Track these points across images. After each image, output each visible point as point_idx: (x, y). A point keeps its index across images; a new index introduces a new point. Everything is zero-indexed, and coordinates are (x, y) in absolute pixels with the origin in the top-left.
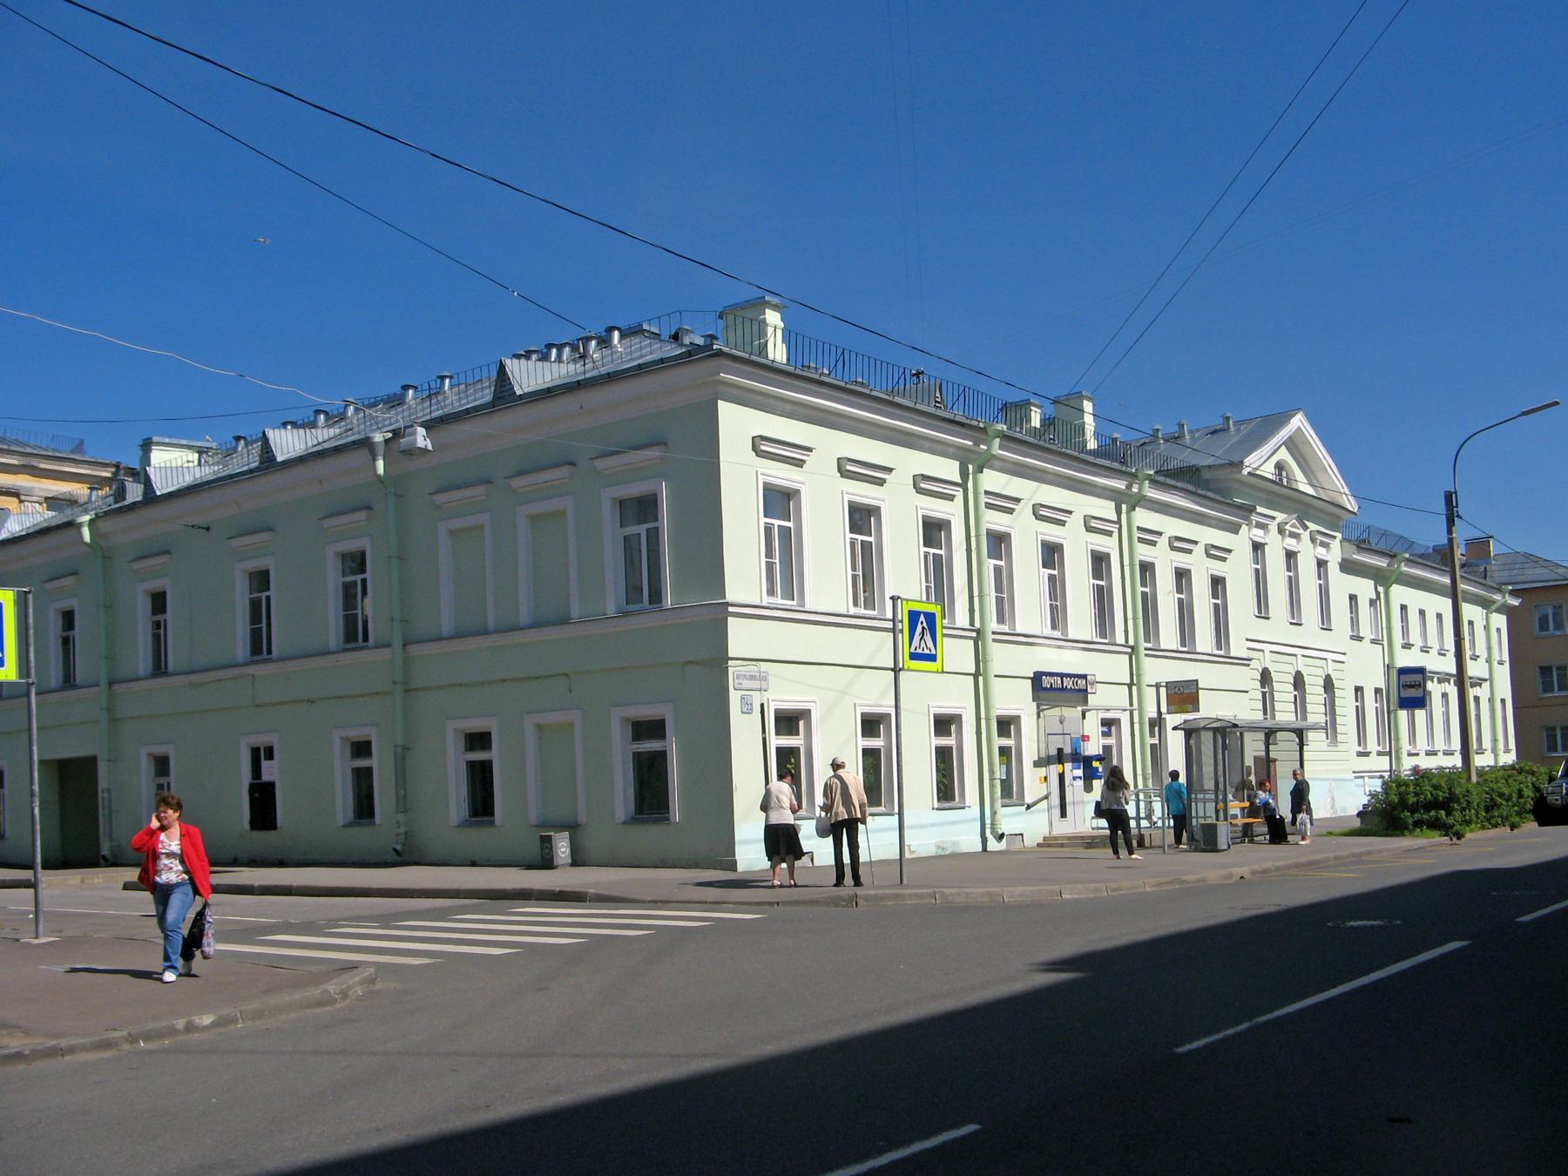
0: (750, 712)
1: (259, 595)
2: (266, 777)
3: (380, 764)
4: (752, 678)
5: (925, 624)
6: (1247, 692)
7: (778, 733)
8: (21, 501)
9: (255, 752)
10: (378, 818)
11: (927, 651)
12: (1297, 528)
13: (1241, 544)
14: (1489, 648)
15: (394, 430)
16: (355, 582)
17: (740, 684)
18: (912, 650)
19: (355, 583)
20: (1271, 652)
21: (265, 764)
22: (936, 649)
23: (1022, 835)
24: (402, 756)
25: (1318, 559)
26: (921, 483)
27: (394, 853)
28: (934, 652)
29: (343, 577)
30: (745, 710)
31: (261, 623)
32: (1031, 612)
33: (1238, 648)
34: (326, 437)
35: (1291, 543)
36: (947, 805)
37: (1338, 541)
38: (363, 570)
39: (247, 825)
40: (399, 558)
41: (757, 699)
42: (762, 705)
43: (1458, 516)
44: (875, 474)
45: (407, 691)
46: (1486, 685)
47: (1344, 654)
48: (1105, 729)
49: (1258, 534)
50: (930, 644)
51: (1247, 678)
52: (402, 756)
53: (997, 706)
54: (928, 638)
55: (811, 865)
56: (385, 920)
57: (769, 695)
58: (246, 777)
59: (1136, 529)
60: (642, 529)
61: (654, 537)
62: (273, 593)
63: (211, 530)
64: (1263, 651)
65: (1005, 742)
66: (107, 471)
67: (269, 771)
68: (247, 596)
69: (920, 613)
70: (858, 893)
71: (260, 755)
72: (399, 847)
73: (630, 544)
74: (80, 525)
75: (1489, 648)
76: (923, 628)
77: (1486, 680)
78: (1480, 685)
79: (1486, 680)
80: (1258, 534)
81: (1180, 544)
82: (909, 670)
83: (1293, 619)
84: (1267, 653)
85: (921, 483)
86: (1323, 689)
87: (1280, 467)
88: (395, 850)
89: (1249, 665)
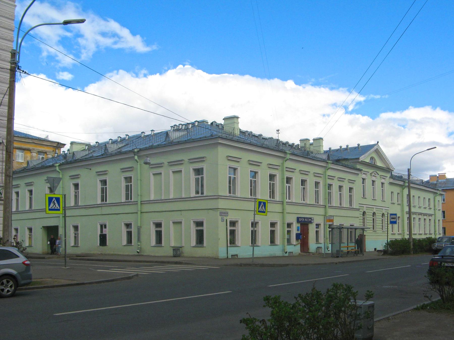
0: (223, 221)
1: (104, 187)
2: (104, 233)
3: (134, 230)
4: (224, 213)
5: (263, 205)
6: (358, 217)
7: (230, 226)
8: (31, 153)
9: (101, 226)
10: (133, 244)
11: (263, 211)
12: (376, 175)
13: (358, 179)
14: (435, 206)
15: (140, 149)
16: (129, 185)
17: (221, 215)
18: (259, 210)
19: (129, 185)
20: (366, 207)
21: (104, 229)
22: (265, 210)
23: (292, 252)
24: (139, 229)
25: (382, 182)
26: (270, 166)
27: (137, 252)
28: (265, 211)
29: (126, 183)
30: (222, 221)
31: (104, 194)
32: (296, 197)
33: (355, 206)
34: (120, 146)
35: (374, 178)
36: (273, 244)
37: (388, 178)
38: (131, 182)
39: (99, 245)
40: (140, 180)
41: (225, 218)
42: (227, 220)
43: (411, 175)
44: (257, 164)
45: (141, 213)
46: (433, 216)
47: (389, 208)
48: (317, 226)
49: (364, 176)
50: (264, 209)
51: (358, 214)
52: (139, 229)
53: (287, 220)
54: (263, 207)
55: (237, 257)
56: (137, 267)
57: (228, 217)
58: (99, 233)
59: (327, 176)
60: (200, 177)
61: (202, 178)
62: (107, 186)
63: (91, 170)
64: (364, 207)
65: (289, 229)
66: (55, 144)
67: (106, 231)
68: (101, 187)
69: (262, 202)
70: (61, 226)
71: (103, 226)
72: (138, 251)
73: (197, 180)
74: (56, 166)
75: (435, 206)
76: (262, 205)
77: (433, 215)
78: (431, 216)
79: (433, 215)
80: (364, 176)
81: (341, 179)
82: (258, 214)
83: (374, 198)
84: (365, 207)
85: (270, 166)
86: (381, 217)
87: (372, 158)
88: (137, 252)
89: (359, 210)
